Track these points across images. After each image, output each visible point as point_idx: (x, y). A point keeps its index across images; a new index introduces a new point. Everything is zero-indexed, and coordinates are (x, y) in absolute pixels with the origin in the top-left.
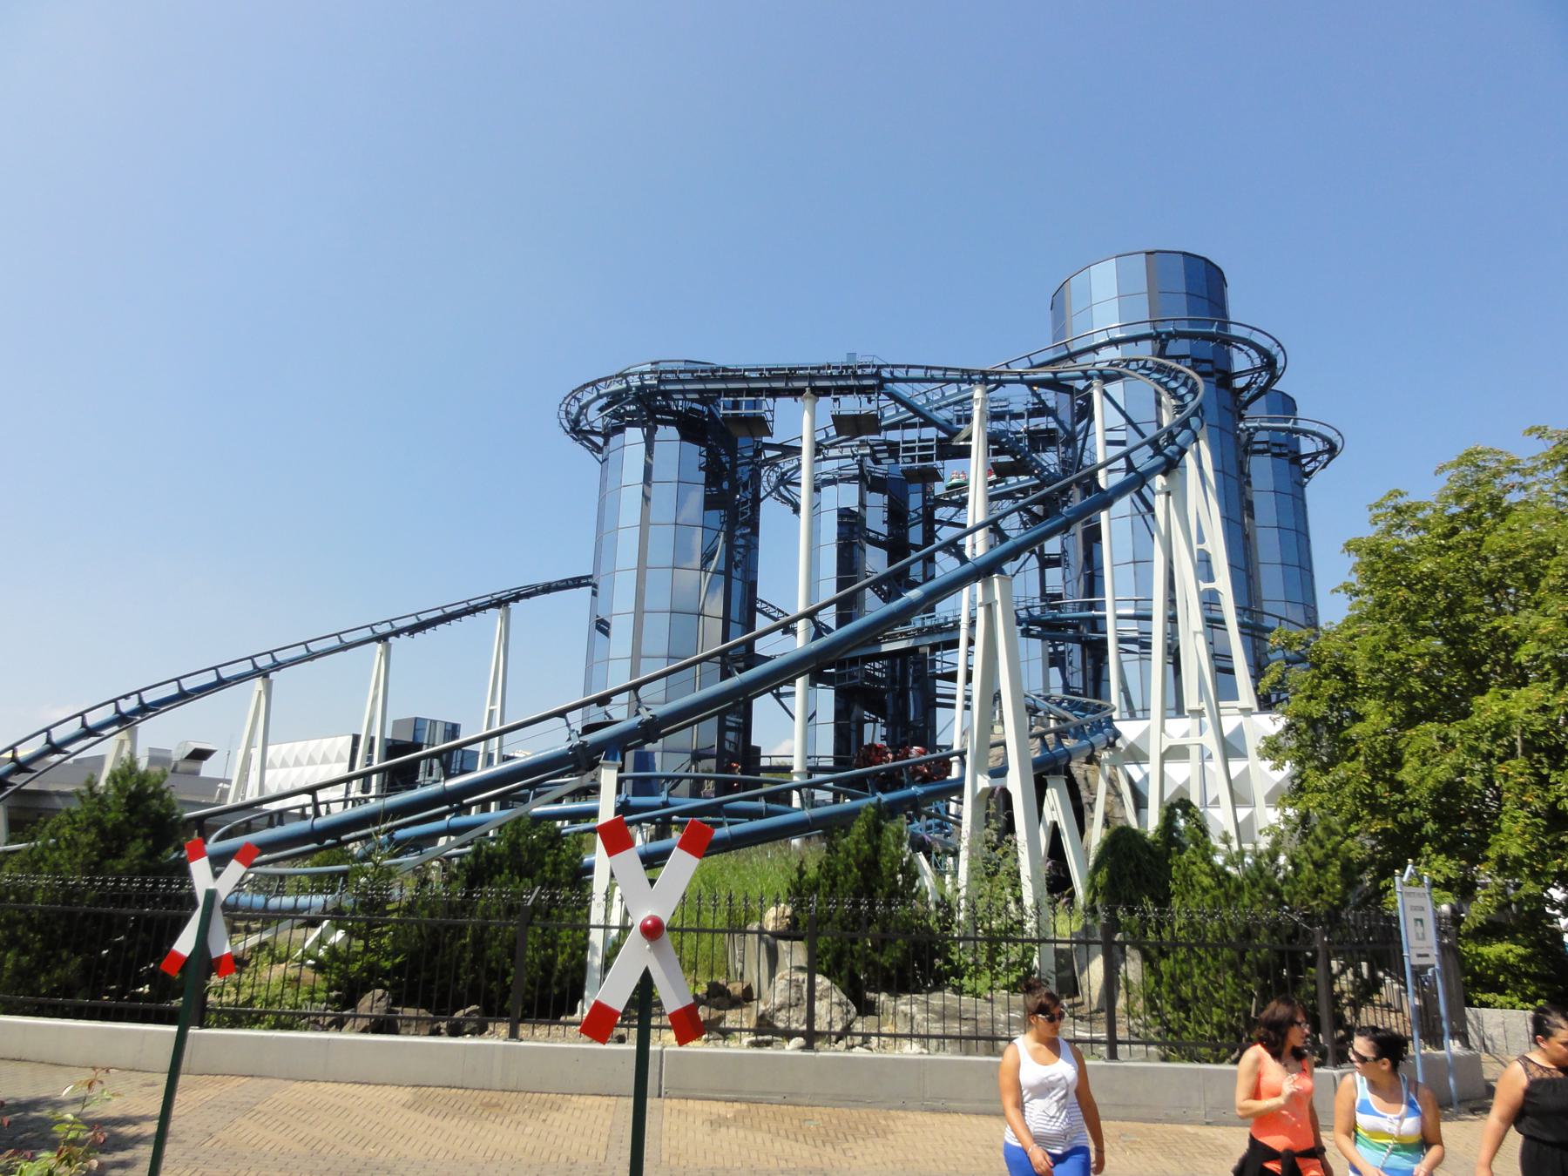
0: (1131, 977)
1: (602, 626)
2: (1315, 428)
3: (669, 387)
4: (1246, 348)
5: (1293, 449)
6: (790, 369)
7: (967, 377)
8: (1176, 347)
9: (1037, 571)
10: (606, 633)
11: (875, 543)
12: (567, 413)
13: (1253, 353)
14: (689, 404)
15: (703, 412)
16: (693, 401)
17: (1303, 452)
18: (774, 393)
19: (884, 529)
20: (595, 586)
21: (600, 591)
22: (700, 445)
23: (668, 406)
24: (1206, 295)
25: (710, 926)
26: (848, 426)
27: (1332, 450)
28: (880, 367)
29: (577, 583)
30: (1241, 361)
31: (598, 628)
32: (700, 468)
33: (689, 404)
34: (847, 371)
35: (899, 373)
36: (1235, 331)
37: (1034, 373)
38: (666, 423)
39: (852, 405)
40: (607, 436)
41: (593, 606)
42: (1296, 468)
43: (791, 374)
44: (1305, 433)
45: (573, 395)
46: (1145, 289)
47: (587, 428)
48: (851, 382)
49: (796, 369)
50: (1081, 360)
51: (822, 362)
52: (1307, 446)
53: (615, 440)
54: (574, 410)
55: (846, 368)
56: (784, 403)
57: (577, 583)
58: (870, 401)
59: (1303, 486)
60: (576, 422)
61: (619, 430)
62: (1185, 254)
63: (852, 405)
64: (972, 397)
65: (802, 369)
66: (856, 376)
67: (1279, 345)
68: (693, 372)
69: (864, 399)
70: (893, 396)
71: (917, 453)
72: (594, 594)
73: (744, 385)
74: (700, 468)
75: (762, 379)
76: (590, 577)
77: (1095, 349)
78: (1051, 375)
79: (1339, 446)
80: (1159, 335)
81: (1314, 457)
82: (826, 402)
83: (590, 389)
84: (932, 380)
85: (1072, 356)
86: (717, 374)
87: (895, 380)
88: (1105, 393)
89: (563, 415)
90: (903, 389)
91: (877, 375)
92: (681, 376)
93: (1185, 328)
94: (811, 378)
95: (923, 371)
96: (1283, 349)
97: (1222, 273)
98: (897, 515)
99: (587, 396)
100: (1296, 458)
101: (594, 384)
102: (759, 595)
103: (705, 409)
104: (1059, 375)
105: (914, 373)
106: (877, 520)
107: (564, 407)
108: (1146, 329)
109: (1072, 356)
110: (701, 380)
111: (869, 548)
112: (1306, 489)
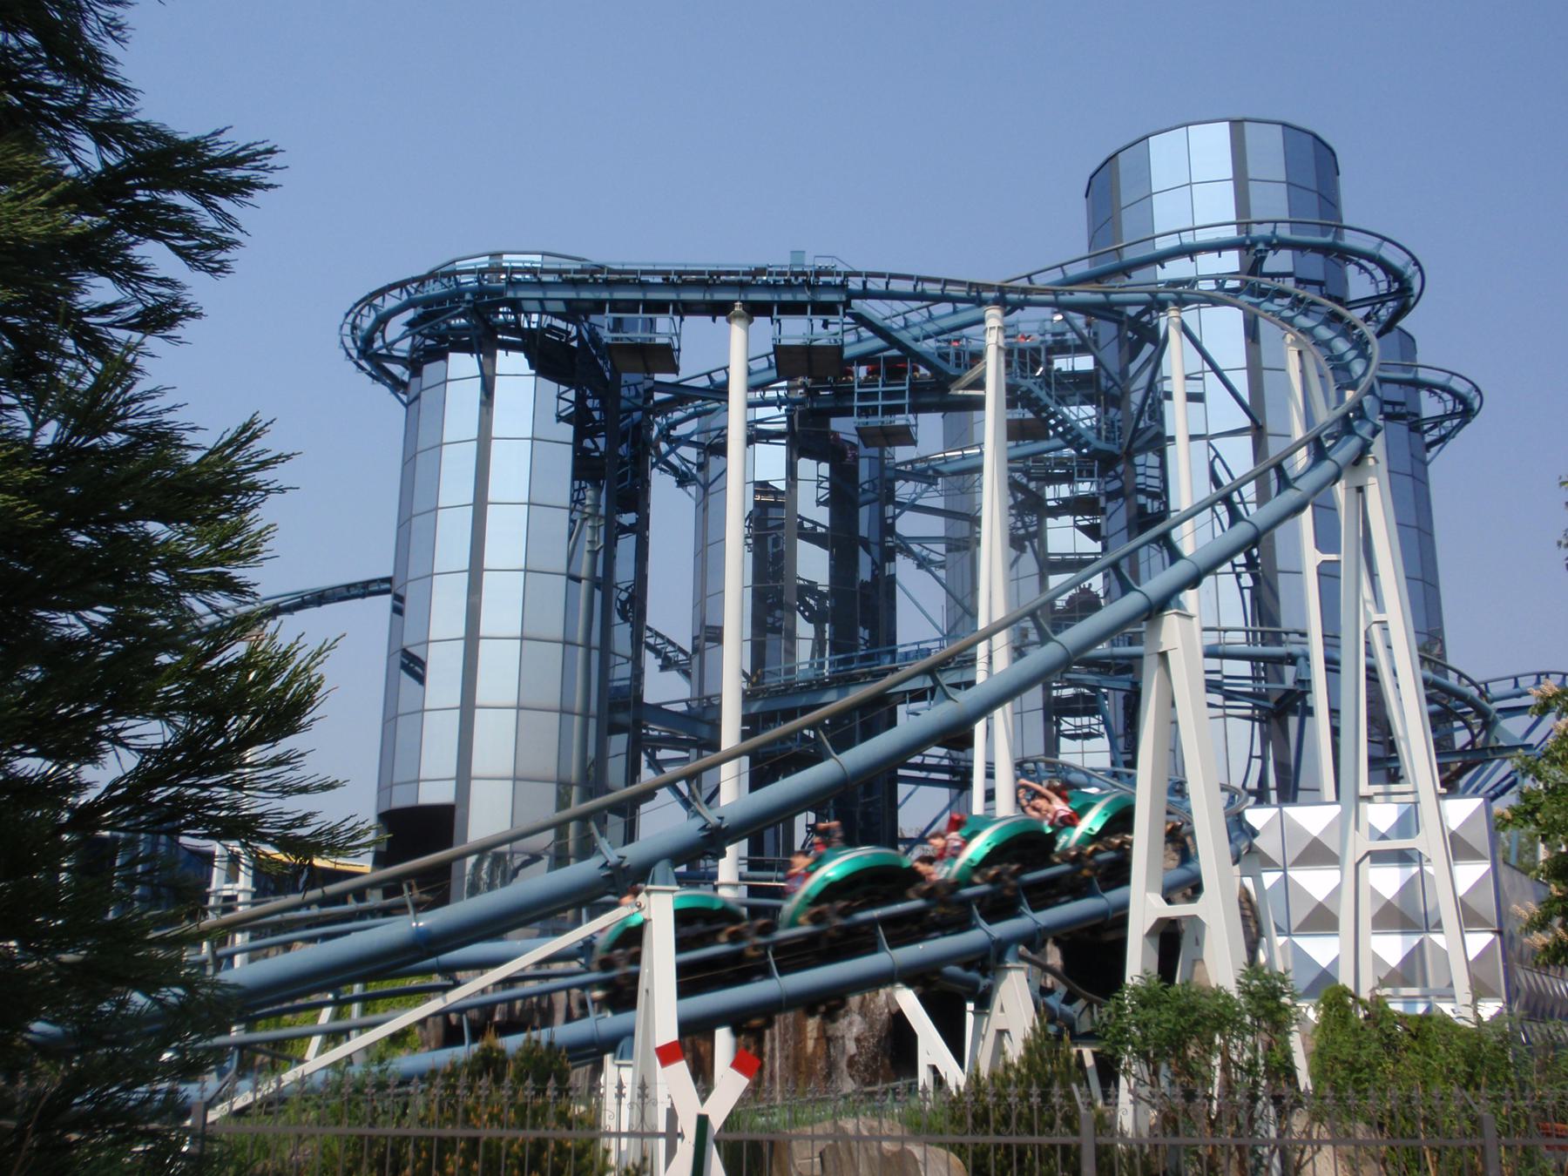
0: (1126, 1128)
1: (413, 665)
2: (1439, 378)
3: (521, 294)
4: (1371, 266)
5: (1412, 410)
6: (711, 274)
7: (976, 295)
8: (1278, 261)
9: (1036, 578)
10: (421, 679)
11: (812, 537)
12: (354, 327)
13: (1379, 274)
14: (547, 320)
15: (568, 333)
16: (556, 315)
17: (1425, 415)
18: (685, 309)
19: (822, 516)
20: (399, 598)
21: (408, 607)
22: (560, 382)
23: (518, 322)
24: (1314, 187)
25: (613, 1129)
26: (787, 360)
27: (1465, 411)
28: (847, 275)
29: (363, 590)
30: (1360, 284)
31: (405, 667)
32: (714, 320)
33: (547, 320)
34: (809, 280)
35: (876, 285)
36: (1350, 240)
37: (1071, 293)
38: (509, 347)
39: (796, 330)
40: (415, 364)
41: (395, 632)
42: (1416, 436)
43: (709, 280)
44: (1431, 387)
45: (368, 300)
46: (1230, 175)
47: (384, 351)
48: (803, 297)
49: (719, 274)
50: (1139, 276)
51: (760, 262)
52: (1430, 406)
53: (431, 370)
54: (367, 323)
55: (796, 275)
56: (695, 325)
57: (363, 590)
58: (825, 325)
59: (1425, 464)
60: (368, 340)
61: (439, 354)
62: (1285, 125)
63: (796, 330)
64: (981, 321)
65: (728, 273)
66: (644, 285)
67: (1417, 263)
68: (560, 272)
69: (818, 321)
70: (861, 320)
71: (880, 402)
72: (398, 611)
73: (636, 295)
74: (819, 503)
75: (668, 284)
76: (388, 580)
77: (1161, 259)
78: (1100, 297)
79: (1476, 405)
80: (1254, 243)
81: (1438, 421)
82: (761, 322)
83: (396, 292)
84: (921, 296)
85: (1126, 269)
86: (593, 276)
87: (866, 294)
88: (1185, 329)
89: (347, 329)
90: (876, 309)
91: (843, 287)
92: (546, 278)
93: (1284, 232)
94: (742, 286)
95: (912, 283)
96: (1421, 269)
97: (1334, 154)
98: (842, 496)
99: (391, 302)
100: (1416, 425)
101: (402, 285)
102: (650, 622)
103: (573, 330)
104: (1114, 297)
105: (897, 286)
106: (811, 506)
107: (350, 319)
108: (1231, 233)
109: (1126, 269)
110: (574, 284)
111: (803, 546)
112: (1430, 468)
